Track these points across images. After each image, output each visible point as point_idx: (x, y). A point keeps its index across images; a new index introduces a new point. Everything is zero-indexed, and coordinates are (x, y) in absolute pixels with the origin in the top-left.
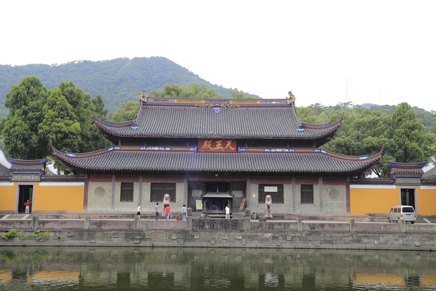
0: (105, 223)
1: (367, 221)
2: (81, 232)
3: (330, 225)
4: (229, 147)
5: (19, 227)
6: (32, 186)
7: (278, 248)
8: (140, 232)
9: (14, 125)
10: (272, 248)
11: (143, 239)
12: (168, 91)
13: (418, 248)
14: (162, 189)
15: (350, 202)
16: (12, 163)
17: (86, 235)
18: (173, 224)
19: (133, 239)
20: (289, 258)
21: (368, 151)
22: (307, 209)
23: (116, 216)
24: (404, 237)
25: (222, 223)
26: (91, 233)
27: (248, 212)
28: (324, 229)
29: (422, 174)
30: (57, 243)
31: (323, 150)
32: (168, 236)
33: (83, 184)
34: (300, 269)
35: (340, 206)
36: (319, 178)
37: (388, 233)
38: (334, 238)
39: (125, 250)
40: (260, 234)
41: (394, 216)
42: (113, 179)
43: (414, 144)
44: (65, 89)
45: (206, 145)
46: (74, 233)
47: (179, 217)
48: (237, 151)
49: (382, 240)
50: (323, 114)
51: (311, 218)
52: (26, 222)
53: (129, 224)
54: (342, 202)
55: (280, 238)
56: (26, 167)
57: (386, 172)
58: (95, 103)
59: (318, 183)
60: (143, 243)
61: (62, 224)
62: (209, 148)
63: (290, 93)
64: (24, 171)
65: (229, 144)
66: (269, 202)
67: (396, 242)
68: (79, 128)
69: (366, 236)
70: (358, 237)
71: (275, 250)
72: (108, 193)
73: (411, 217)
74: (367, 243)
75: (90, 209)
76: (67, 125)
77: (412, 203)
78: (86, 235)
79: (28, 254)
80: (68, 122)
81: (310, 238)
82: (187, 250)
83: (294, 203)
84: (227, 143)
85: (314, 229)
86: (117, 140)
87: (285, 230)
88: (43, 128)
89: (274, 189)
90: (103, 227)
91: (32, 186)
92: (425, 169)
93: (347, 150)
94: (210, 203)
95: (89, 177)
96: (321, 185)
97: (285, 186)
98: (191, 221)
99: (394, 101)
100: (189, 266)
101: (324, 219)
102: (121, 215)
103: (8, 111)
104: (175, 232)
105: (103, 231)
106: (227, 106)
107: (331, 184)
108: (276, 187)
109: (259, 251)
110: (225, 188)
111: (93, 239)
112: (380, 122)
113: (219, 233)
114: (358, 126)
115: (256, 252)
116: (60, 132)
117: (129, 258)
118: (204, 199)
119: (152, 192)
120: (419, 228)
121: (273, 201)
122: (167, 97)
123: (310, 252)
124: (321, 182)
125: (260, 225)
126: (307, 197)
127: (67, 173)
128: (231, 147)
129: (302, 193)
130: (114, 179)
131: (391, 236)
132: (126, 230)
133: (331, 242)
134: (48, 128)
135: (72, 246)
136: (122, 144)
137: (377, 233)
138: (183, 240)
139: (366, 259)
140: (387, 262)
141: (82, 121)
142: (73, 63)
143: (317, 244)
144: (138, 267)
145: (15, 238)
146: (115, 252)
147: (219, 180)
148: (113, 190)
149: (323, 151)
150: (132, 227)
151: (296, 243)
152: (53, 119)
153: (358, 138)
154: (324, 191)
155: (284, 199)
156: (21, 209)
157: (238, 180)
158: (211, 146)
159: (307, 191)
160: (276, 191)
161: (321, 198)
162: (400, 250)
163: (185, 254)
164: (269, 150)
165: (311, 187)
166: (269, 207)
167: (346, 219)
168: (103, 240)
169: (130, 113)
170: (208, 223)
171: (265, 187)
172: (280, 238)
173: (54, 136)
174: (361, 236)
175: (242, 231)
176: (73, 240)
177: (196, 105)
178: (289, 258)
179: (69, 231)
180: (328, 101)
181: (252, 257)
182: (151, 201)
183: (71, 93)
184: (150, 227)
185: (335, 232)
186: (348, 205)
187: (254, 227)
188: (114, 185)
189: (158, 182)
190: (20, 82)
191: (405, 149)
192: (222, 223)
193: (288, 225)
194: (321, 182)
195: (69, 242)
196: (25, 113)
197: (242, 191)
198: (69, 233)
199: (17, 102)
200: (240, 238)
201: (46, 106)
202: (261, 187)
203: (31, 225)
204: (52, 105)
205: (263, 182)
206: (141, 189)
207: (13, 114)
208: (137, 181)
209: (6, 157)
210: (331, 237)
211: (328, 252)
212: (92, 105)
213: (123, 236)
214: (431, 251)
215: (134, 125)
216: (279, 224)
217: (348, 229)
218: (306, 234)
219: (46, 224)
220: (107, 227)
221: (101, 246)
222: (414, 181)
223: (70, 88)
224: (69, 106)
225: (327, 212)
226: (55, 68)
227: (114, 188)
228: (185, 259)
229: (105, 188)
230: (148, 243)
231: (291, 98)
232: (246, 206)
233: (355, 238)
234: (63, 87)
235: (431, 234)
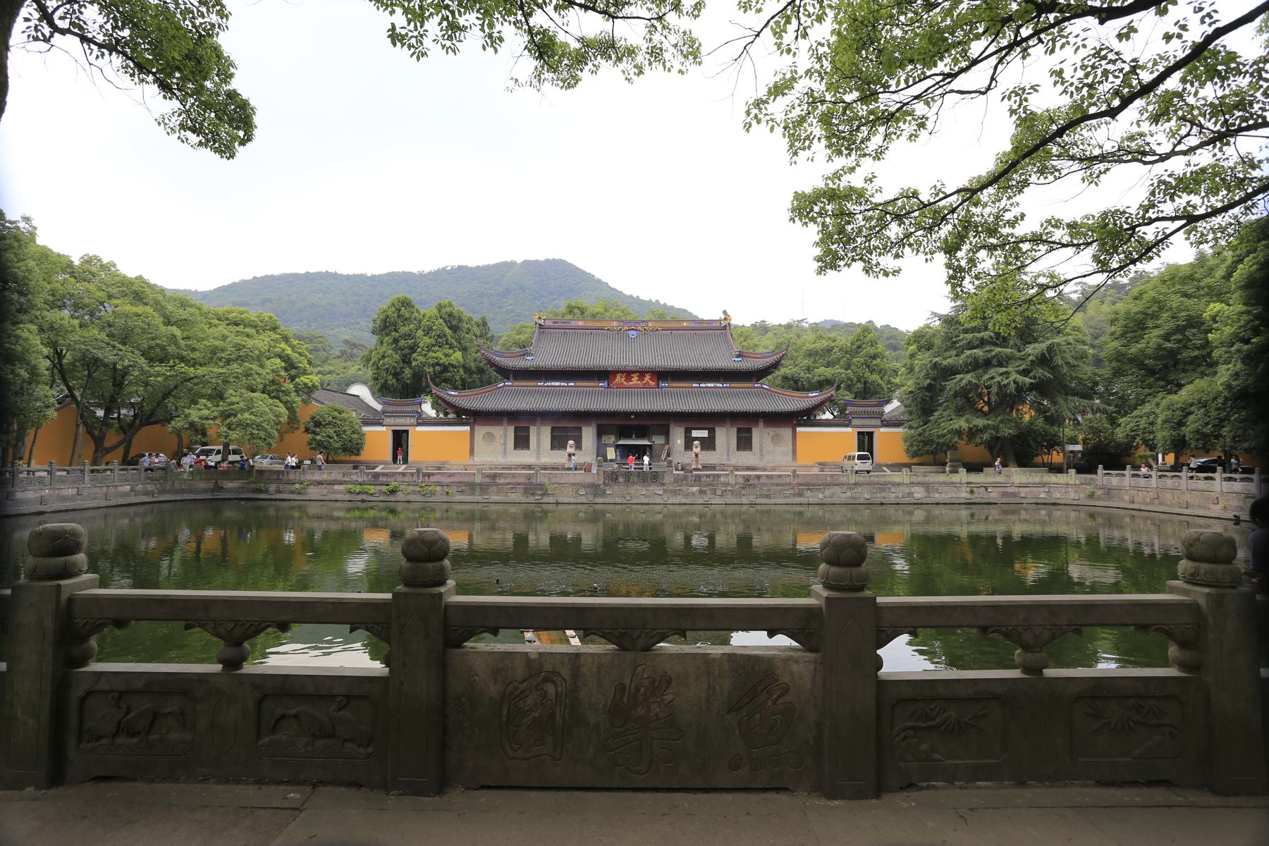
0: (500, 475)
1: (816, 471)
2: (472, 487)
3: (767, 476)
7: (706, 504)
8: (541, 486)
9: (383, 357)
11: (545, 494)
12: (571, 310)
16: (384, 403)
17: (478, 490)
18: (580, 476)
19: (533, 494)
20: (719, 516)
21: (821, 385)
22: (745, 458)
25: (639, 475)
26: (484, 488)
27: (670, 462)
29: (882, 413)
30: (445, 498)
31: (765, 384)
34: (732, 528)
41: (848, 464)
43: (875, 377)
44: (443, 311)
45: (619, 379)
47: (588, 469)
49: (827, 492)
50: (770, 334)
51: (748, 469)
53: (529, 477)
56: (399, 409)
57: (842, 411)
58: (478, 326)
60: (545, 500)
63: (725, 312)
65: (647, 378)
66: (697, 450)
68: (461, 359)
71: (701, 507)
73: (867, 465)
74: (810, 497)
75: (479, 459)
76: (446, 355)
77: (871, 450)
78: (478, 490)
79: (414, 511)
80: (448, 351)
82: (597, 507)
86: (506, 373)
88: (418, 359)
89: (704, 434)
92: (888, 409)
93: (795, 384)
94: (625, 451)
99: (860, 319)
100: (601, 525)
101: (765, 470)
103: (374, 339)
104: (583, 486)
105: (498, 485)
110: (643, 432)
112: (836, 350)
114: (810, 354)
115: (679, 509)
116: (438, 364)
117: (530, 517)
118: (617, 447)
119: (553, 438)
121: (702, 449)
122: (569, 317)
123: (744, 508)
124: (761, 424)
125: (685, 478)
126: (744, 443)
127: (446, 414)
129: (739, 439)
130: (505, 422)
131: (838, 490)
133: (768, 496)
134: (423, 360)
136: (515, 379)
141: (464, 349)
142: (444, 269)
143: (752, 499)
144: (540, 527)
146: (513, 509)
147: (636, 423)
148: (505, 435)
152: (429, 348)
153: (808, 369)
154: (766, 436)
156: (395, 460)
157: (659, 422)
161: (761, 445)
163: (595, 511)
165: (749, 431)
166: (697, 455)
169: (522, 337)
173: (431, 370)
175: (663, 484)
178: (719, 516)
180: (777, 316)
181: (675, 515)
183: (450, 315)
184: (553, 481)
186: (794, 452)
187: (677, 480)
188: (506, 430)
190: (389, 302)
191: (866, 383)
192: (639, 475)
194: (761, 424)
195: (459, 498)
196: (396, 341)
199: (386, 327)
201: (420, 333)
202: (688, 431)
203: (415, 478)
204: (428, 331)
206: (539, 435)
207: (382, 343)
209: (373, 394)
211: (764, 508)
212: (475, 329)
215: (529, 354)
216: (708, 476)
220: (502, 481)
222: (874, 422)
223: (448, 309)
224: (448, 331)
225: (768, 461)
227: (507, 433)
228: (595, 517)
230: (551, 499)
232: (669, 455)
234: (440, 307)
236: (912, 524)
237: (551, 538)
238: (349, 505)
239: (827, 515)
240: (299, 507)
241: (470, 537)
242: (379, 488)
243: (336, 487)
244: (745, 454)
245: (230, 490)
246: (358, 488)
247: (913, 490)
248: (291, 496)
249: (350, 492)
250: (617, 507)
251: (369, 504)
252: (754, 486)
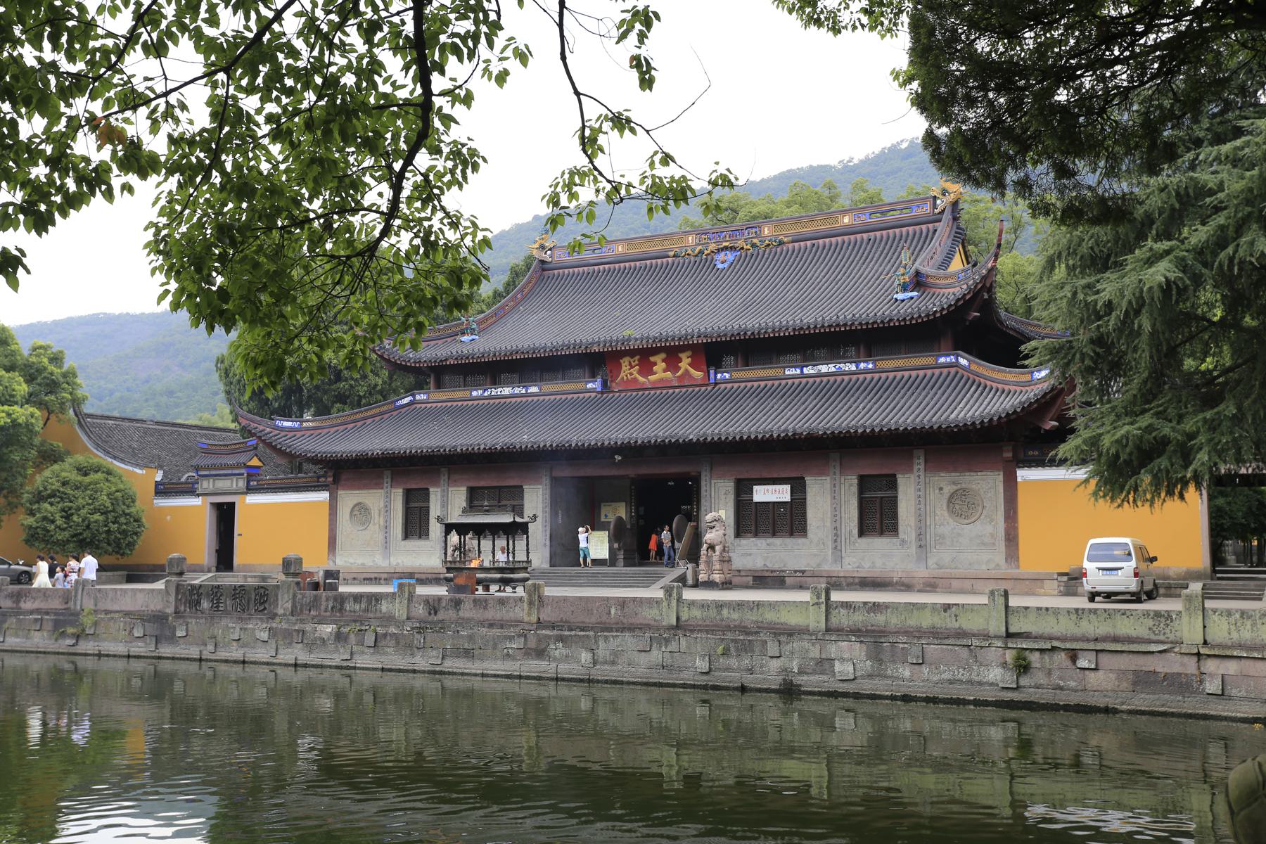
4: (686, 370)
6: (233, 504)
10: (330, 667)
13: (705, 678)
15: (1016, 529)
20: (368, 698)
22: (877, 555)
24: (667, 641)
28: (461, 614)
33: (324, 496)
35: (983, 544)
36: (915, 452)
37: (623, 630)
45: (628, 370)
62: (635, 378)
64: (222, 467)
65: (685, 362)
67: (644, 659)
69: (561, 639)
70: (539, 641)
83: (836, 535)
85: (436, 613)
87: (371, 615)
90: (22, 605)
91: (233, 504)
95: (336, 481)
96: (922, 473)
97: (809, 480)
106: (754, 245)
107: (955, 471)
108: (787, 488)
113: (224, 622)
120: (719, 613)
123: (419, 682)
125: (315, 603)
126: (877, 516)
128: (692, 371)
130: (387, 481)
131: (628, 641)
132: (56, 612)
133: (468, 654)
136: (439, 385)
137: (592, 629)
139: (557, 709)
140: (614, 720)
142: (894, 149)
148: (387, 509)
150: (71, 604)
151: (386, 654)
154: (933, 495)
155: (808, 522)
158: (640, 373)
159: (880, 494)
160: (787, 498)
161: (921, 518)
162: (654, 684)
164: (798, 371)
165: (892, 483)
167: (979, 585)
170: (208, 595)
171: (755, 488)
174: (549, 637)
177: (671, 254)
181: (288, 690)
182: (862, 533)
185: (481, 624)
186: (1011, 538)
188: (388, 496)
193: (377, 600)
194: (919, 464)
202: (743, 488)
205: (747, 473)
208: (437, 484)
214: (743, 689)
218: (413, 628)
226: (848, 169)
227: (386, 503)
233: (532, 643)
235: (747, 634)
236: (832, 758)
239: (602, 712)
244: (414, 544)
247: (832, 650)
252: (442, 627)
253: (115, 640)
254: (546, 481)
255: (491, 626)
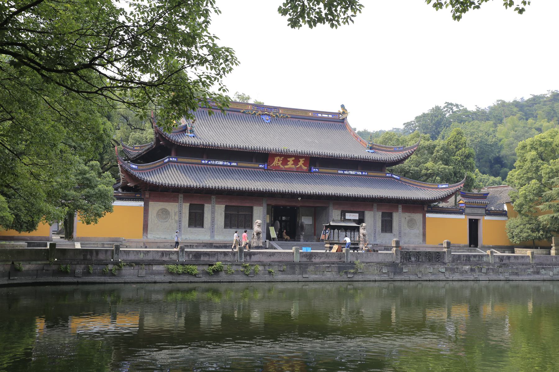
5: (223, 260)
8: (352, 265)
14: (236, 213)
17: (297, 270)
23: (191, 246)
30: (268, 278)
32: (379, 270)
33: (142, 203)
38: (520, 270)
39: (337, 285)
40: (460, 267)
42: (212, 200)
45: (277, 162)
46: (285, 267)
48: (310, 171)
52: (230, 254)
54: (418, 232)
55: (477, 270)
59: (397, 211)
60: (357, 278)
61: (270, 256)
62: (279, 166)
63: (343, 106)
69: (543, 268)
70: (537, 268)
72: (173, 216)
75: (151, 237)
78: (297, 270)
79: (237, 291)
81: (501, 270)
84: (299, 161)
87: (480, 262)
90: (313, 260)
98: (399, 254)
102: (196, 244)
106: (277, 116)
108: (357, 214)
109: (461, 283)
111: (306, 273)
113: (424, 266)
124: (400, 209)
128: (303, 166)
129: (226, 216)
133: (517, 274)
135: (284, 282)
138: (393, 274)
143: (507, 276)
145: (220, 273)
146: (328, 286)
148: (180, 212)
149: (395, 176)
150: (342, 260)
151: (490, 275)
154: (403, 220)
157: (319, 204)
165: (202, 207)
168: (316, 275)
170: (414, 255)
172: (477, 270)
176: (285, 274)
177: (242, 111)
179: (280, 264)
186: (424, 235)
189: (233, 204)
194: (400, 209)
195: (280, 277)
197: (311, 218)
198: (281, 266)
200: (444, 270)
203: (237, 257)
206: (213, 213)
208: (209, 202)
210: (517, 269)
213: (336, 269)
217: (528, 261)
219: (253, 256)
220: (316, 260)
221: (314, 281)
229: (170, 210)
231: (344, 113)
233: (535, 270)
237: (222, 317)
238: (168, 287)
240: (111, 292)
241: (141, 320)
242: (201, 268)
243: (155, 268)
244: (388, 235)
245: (28, 273)
246: (180, 269)
248: (102, 279)
249: (171, 273)
250: (412, 284)
251: (191, 286)
253: (373, 274)
254: (265, 205)
255: (523, 265)
